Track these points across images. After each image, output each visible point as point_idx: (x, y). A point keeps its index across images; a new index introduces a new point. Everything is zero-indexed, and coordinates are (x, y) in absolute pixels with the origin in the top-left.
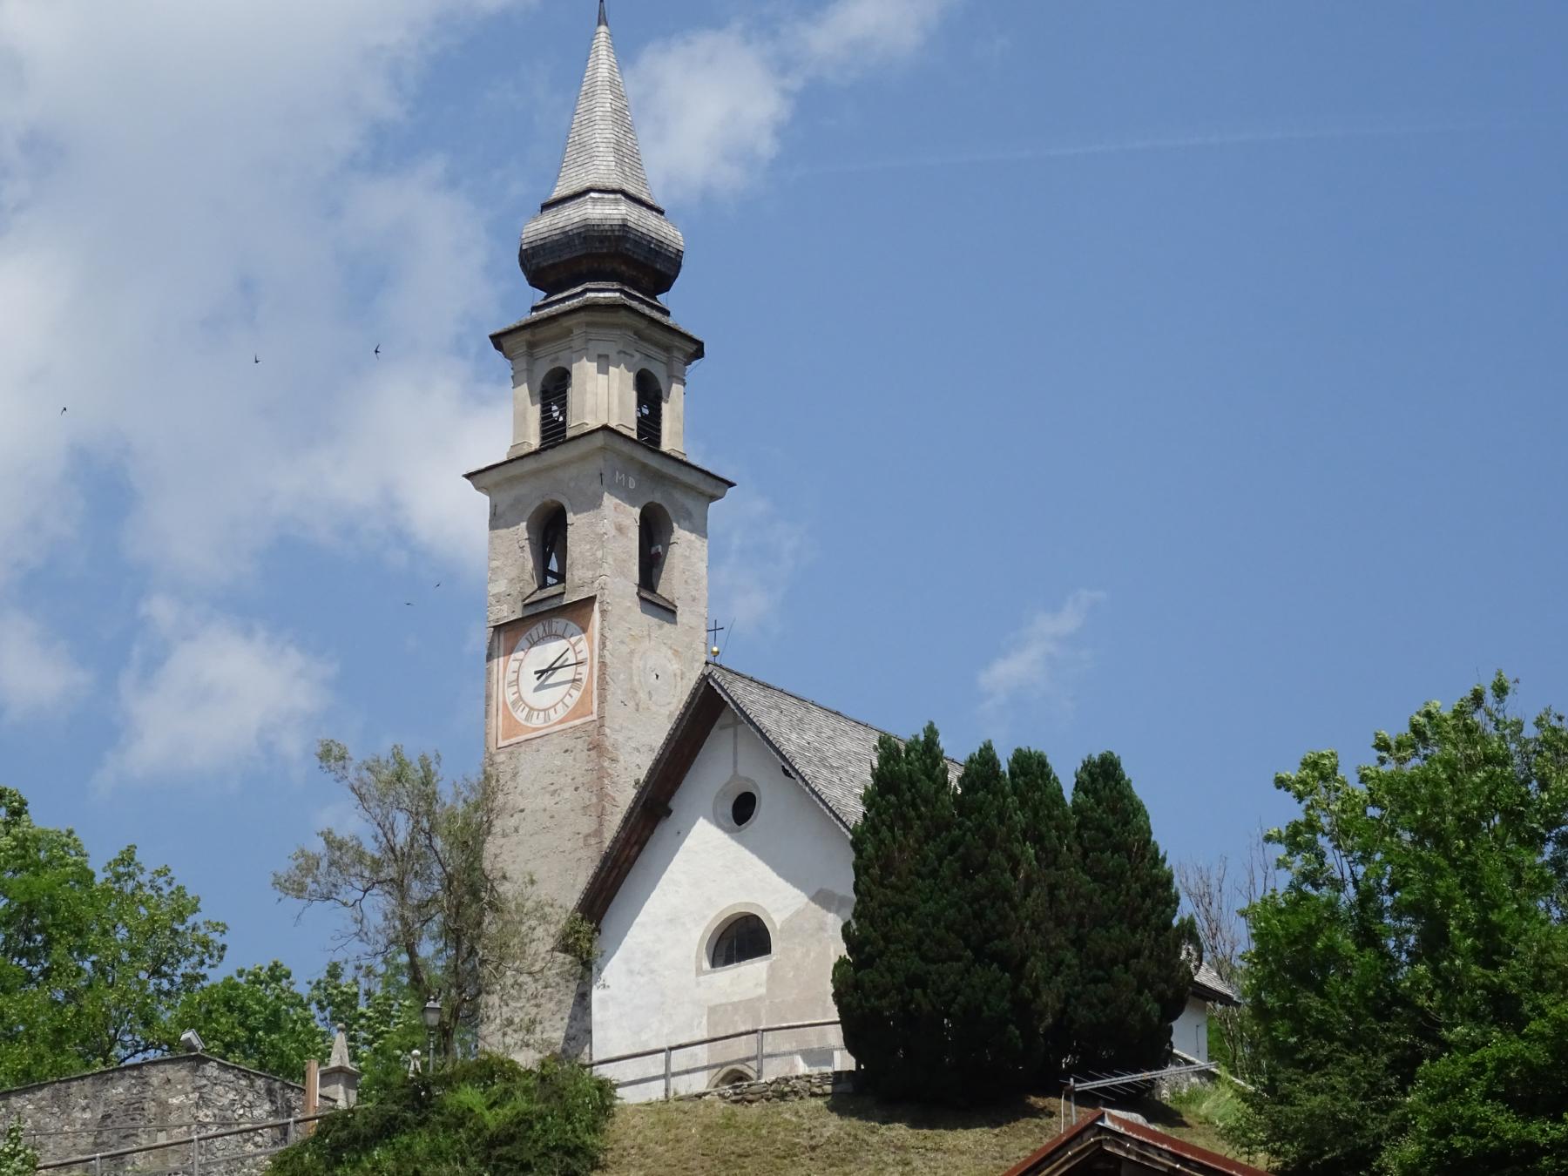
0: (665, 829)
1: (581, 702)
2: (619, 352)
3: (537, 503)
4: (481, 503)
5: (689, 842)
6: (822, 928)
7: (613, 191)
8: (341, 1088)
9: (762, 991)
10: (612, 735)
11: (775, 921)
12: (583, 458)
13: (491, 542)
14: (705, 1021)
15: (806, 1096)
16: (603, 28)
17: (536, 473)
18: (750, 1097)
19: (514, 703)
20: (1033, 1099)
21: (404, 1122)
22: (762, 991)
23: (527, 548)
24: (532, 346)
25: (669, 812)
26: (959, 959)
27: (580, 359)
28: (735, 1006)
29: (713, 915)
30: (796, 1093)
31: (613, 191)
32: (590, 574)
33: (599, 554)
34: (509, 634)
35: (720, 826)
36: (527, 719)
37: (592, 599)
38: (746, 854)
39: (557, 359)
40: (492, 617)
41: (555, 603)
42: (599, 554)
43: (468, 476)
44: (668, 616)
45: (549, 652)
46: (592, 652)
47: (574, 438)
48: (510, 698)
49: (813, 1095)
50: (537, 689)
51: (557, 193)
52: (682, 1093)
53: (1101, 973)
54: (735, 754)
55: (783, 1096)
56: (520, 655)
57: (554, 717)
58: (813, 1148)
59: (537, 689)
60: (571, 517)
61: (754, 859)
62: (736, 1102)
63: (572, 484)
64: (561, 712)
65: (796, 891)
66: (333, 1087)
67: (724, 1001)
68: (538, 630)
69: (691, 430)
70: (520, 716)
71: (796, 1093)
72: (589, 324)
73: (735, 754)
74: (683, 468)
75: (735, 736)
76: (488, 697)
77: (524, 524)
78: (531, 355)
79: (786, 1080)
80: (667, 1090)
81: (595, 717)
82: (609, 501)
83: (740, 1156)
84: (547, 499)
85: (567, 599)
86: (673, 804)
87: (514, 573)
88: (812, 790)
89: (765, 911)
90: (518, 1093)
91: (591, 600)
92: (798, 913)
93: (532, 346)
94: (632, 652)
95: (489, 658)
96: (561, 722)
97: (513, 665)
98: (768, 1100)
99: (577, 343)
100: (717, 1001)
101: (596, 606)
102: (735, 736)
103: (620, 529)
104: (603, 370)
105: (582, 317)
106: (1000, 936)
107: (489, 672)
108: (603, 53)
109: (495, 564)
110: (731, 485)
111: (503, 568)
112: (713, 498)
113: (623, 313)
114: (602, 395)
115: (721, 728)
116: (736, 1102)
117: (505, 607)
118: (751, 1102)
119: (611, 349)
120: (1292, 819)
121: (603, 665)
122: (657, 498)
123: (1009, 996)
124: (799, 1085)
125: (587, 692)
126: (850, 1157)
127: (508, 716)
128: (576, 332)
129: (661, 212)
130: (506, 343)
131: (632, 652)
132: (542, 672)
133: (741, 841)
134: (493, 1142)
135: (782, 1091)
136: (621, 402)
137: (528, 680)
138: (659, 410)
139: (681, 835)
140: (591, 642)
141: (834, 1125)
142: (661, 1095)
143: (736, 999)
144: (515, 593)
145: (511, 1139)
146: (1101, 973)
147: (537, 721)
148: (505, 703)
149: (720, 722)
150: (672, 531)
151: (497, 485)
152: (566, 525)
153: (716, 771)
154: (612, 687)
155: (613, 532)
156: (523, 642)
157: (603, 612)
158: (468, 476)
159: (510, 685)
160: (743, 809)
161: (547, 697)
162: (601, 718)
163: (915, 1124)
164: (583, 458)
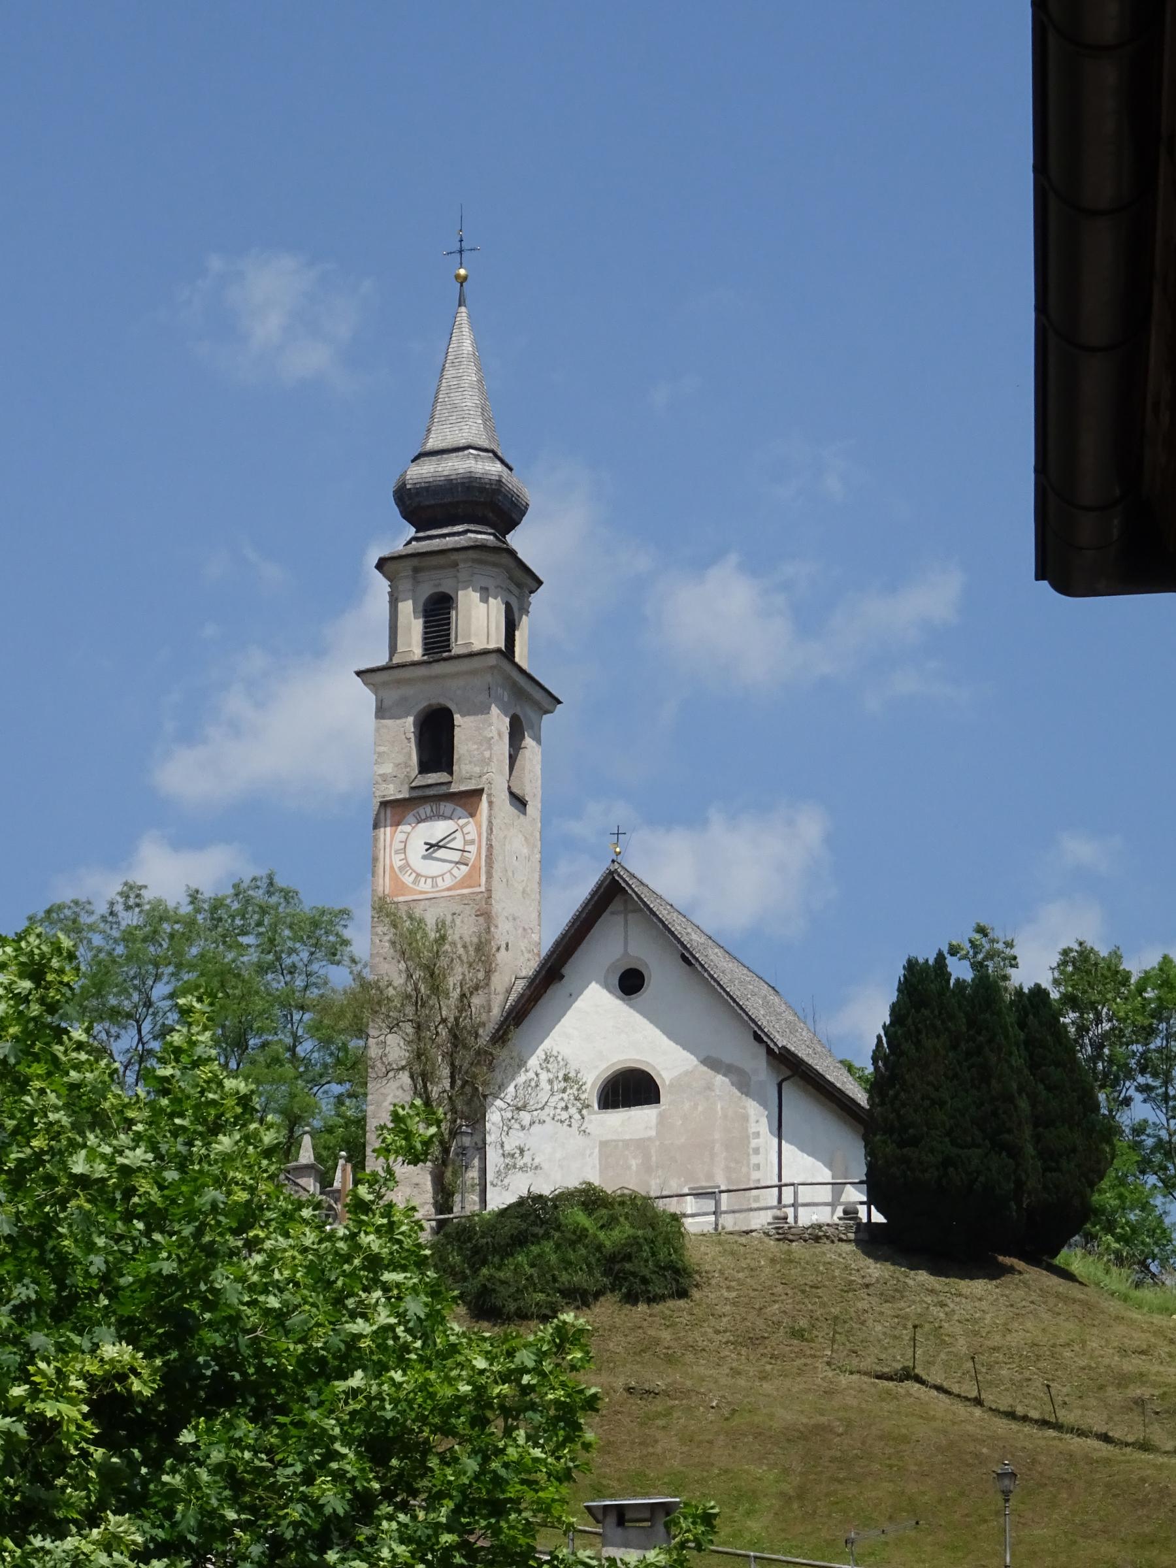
0: (556, 992)
1: (469, 876)
2: (497, 587)
3: (425, 704)
4: (368, 698)
5: (581, 1003)
6: (709, 1087)
7: (486, 450)
8: (312, 1180)
9: (653, 1133)
10: (497, 907)
11: (664, 1076)
12: (473, 672)
13: (377, 730)
14: (597, 1150)
15: (836, 1240)
16: (463, 309)
17: (426, 679)
18: (791, 1237)
19: (401, 868)
20: (1001, 1258)
21: (535, 1235)
22: (653, 1133)
23: (413, 740)
24: (416, 570)
25: (562, 977)
26: (979, 1146)
27: (465, 588)
28: (627, 1143)
29: (604, 1066)
30: (828, 1238)
31: (486, 450)
32: (477, 770)
33: (487, 754)
34: (395, 810)
35: (610, 992)
36: (414, 882)
37: (481, 791)
38: (638, 1017)
39: (440, 585)
40: (378, 793)
41: (443, 790)
42: (487, 754)
43: (359, 673)
44: (521, 806)
45: (438, 829)
46: (480, 835)
47: (458, 657)
48: (397, 861)
49: (841, 1240)
50: (424, 857)
51: (432, 443)
52: (730, 1228)
53: (1053, 1164)
54: (626, 938)
55: (817, 1239)
56: (407, 828)
57: (442, 885)
58: (867, 1286)
59: (424, 857)
60: (458, 719)
61: (645, 1022)
62: (778, 1240)
63: (459, 692)
64: (449, 881)
65: (692, 1057)
66: (305, 1180)
67: (614, 1138)
68: (425, 810)
69: (532, 654)
70: (408, 879)
71: (828, 1238)
72: (474, 561)
73: (626, 932)
74: (534, 685)
75: (626, 921)
76: (375, 860)
77: (411, 719)
78: (414, 578)
79: (820, 1226)
80: (717, 1225)
81: (483, 889)
82: (495, 710)
83: (811, 1287)
84: (434, 701)
85: (454, 788)
86: (564, 971)
87: (401, 759)
88: (712, 977)
89: (654, 1068)
90: (622, 1219)
91: (478, 793)
92: (686, 1073)
93: (416, 570)
94: (505, 838)
95: (376, 826)
96: (449, 889)
97: (400, 836)
98: (805, 1241)
99: (463, 575)
100: (609, 1137)
101: (484, 797)
102: (626, 921)
103: (500, 735)
104: (484, 600)
105: (472, 554)
106: (1009, 1131)
107: (376, 839)
108: (466, 329)
109: (382, 749)
110: (559, 702)
111: (393, 754)
112: (547, 712)
113: (505, 555)
114: (478, 620)
115: (613, 913)
116: (778, 1240)
117: (391, 786)
118: (791, 1241)
119: (490, 583)
120: (163, 898)
121: (490, 847)
122: (518, 711)
123: (1013, 1178)
124: (830, 1231)
125: (475, 868)
126: (898, 1295)
127: (395, 878)
128: (461, 565)
129: (511, 469)
130: (389, 566)
131: (505, 838)
132: (432, 846)
133: (631, 1007)
134: (612, 1259)
135: (816, 1235)
136: (497, 628)
137: (417, 848)
138: (514, 635)
139: (572, 997)
140: (479, 826)
141: (875, 1270)
142: (710, 1228)
143: (627, 1137)
144: (401, 776)
145: (628, 1258)
146: (1053, 1164)
147: (425, 886)
148: (392, 867)
149: (610, 909)
150: (524, 737)
151: (385, 684)
152: (452, 726)
153: (612, 945)
154: (496, 866)
155: (496, 737)
156: (410, 817)
157: (490, 803)
158: (359, 673)
159: (397, 852)
160: (630, 983)
161: (433, 868)
162: (489, 890)
163: (935, 1271)
164: (473, 672)
